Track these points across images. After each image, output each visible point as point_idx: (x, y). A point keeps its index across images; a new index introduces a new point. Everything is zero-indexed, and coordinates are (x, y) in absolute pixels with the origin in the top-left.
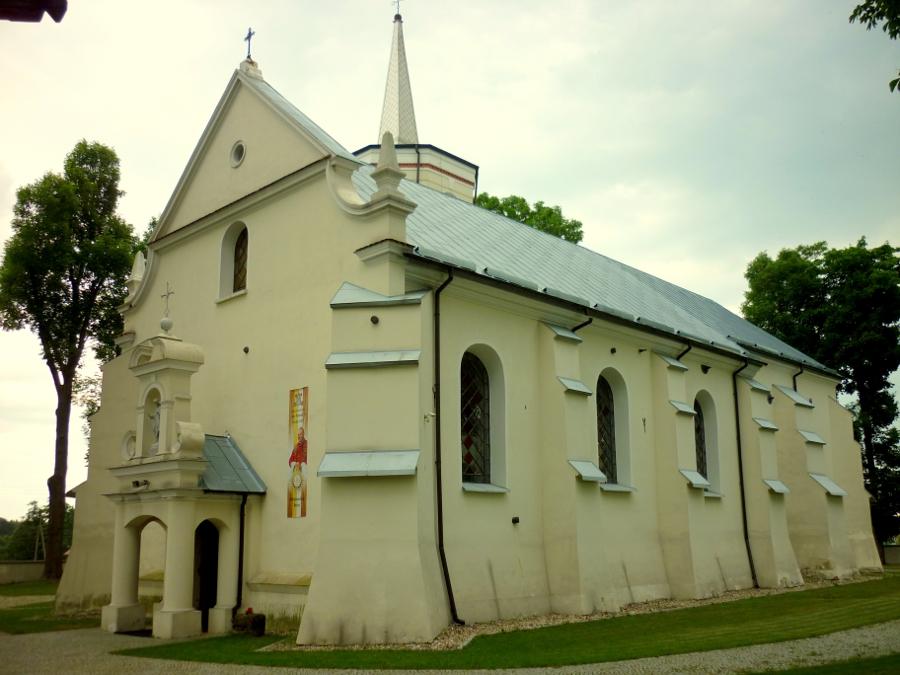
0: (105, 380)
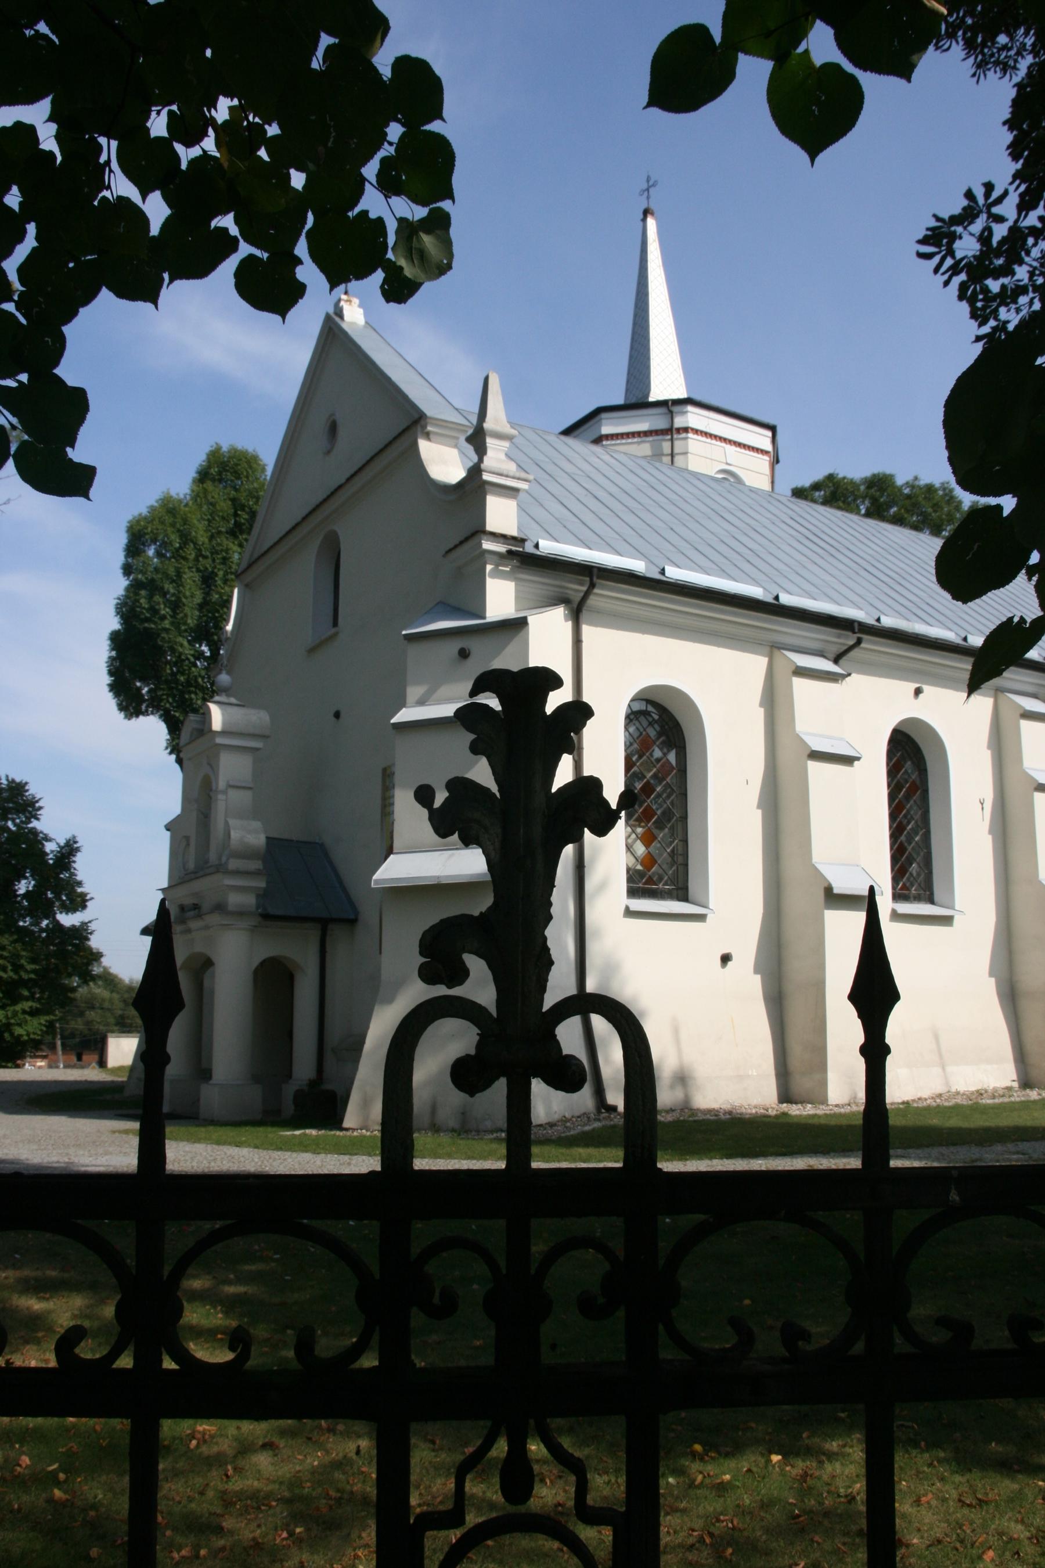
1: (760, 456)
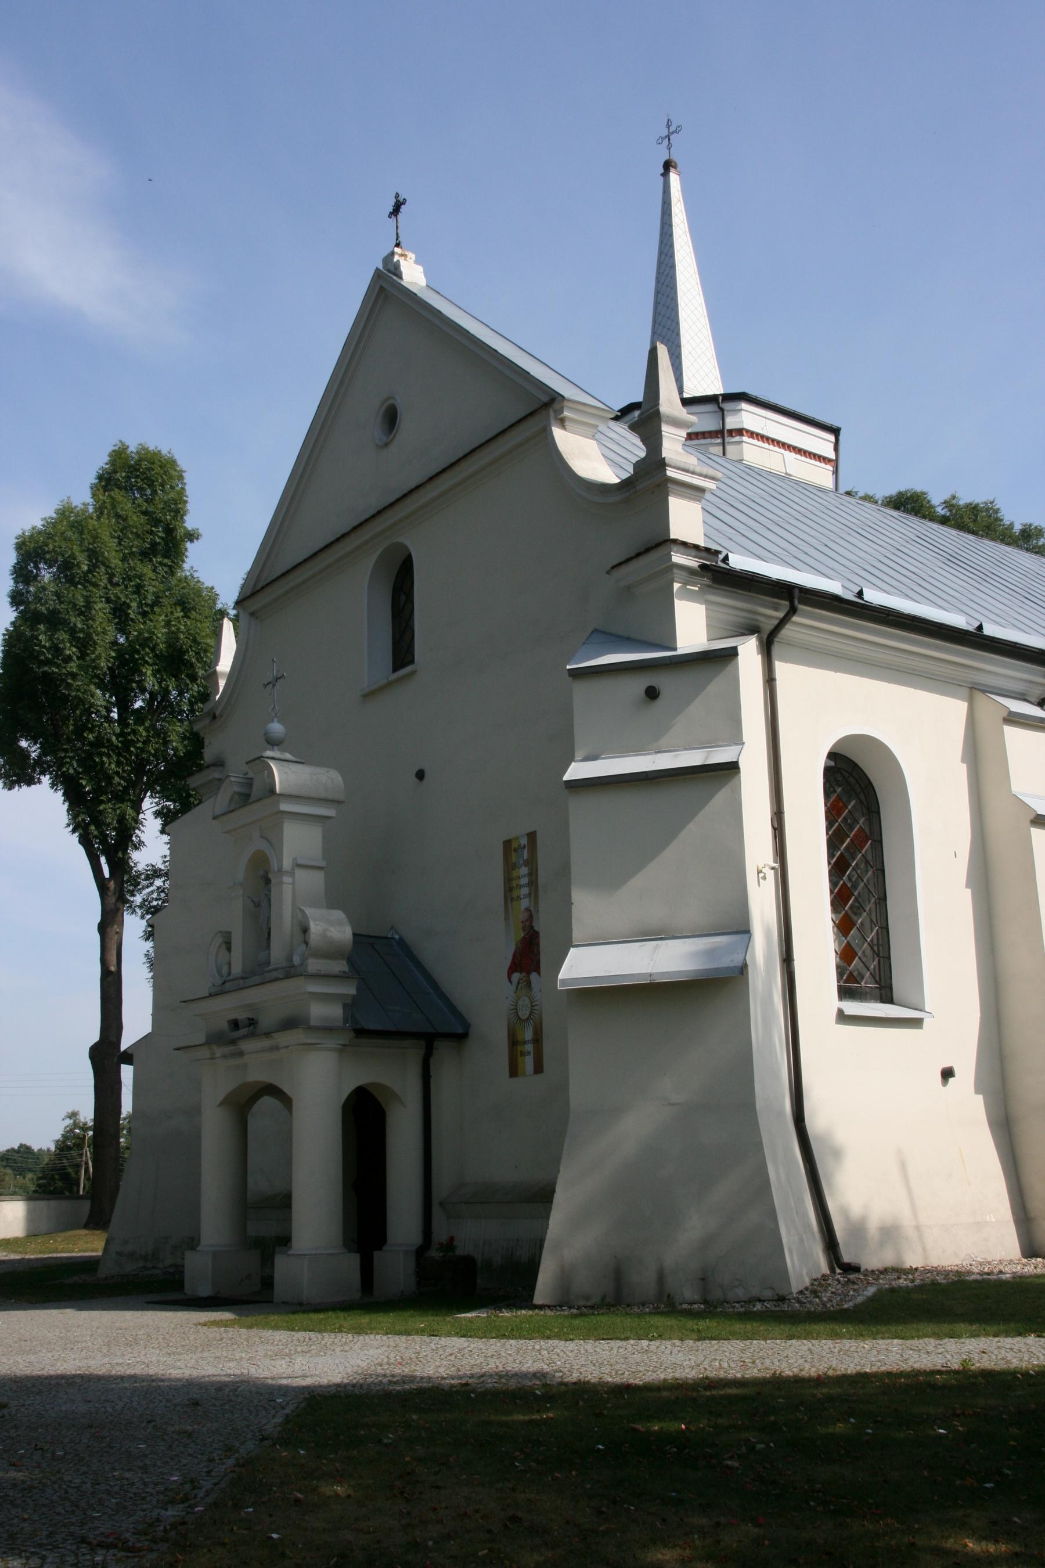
0: (171, 855)
1: (823, 465)
